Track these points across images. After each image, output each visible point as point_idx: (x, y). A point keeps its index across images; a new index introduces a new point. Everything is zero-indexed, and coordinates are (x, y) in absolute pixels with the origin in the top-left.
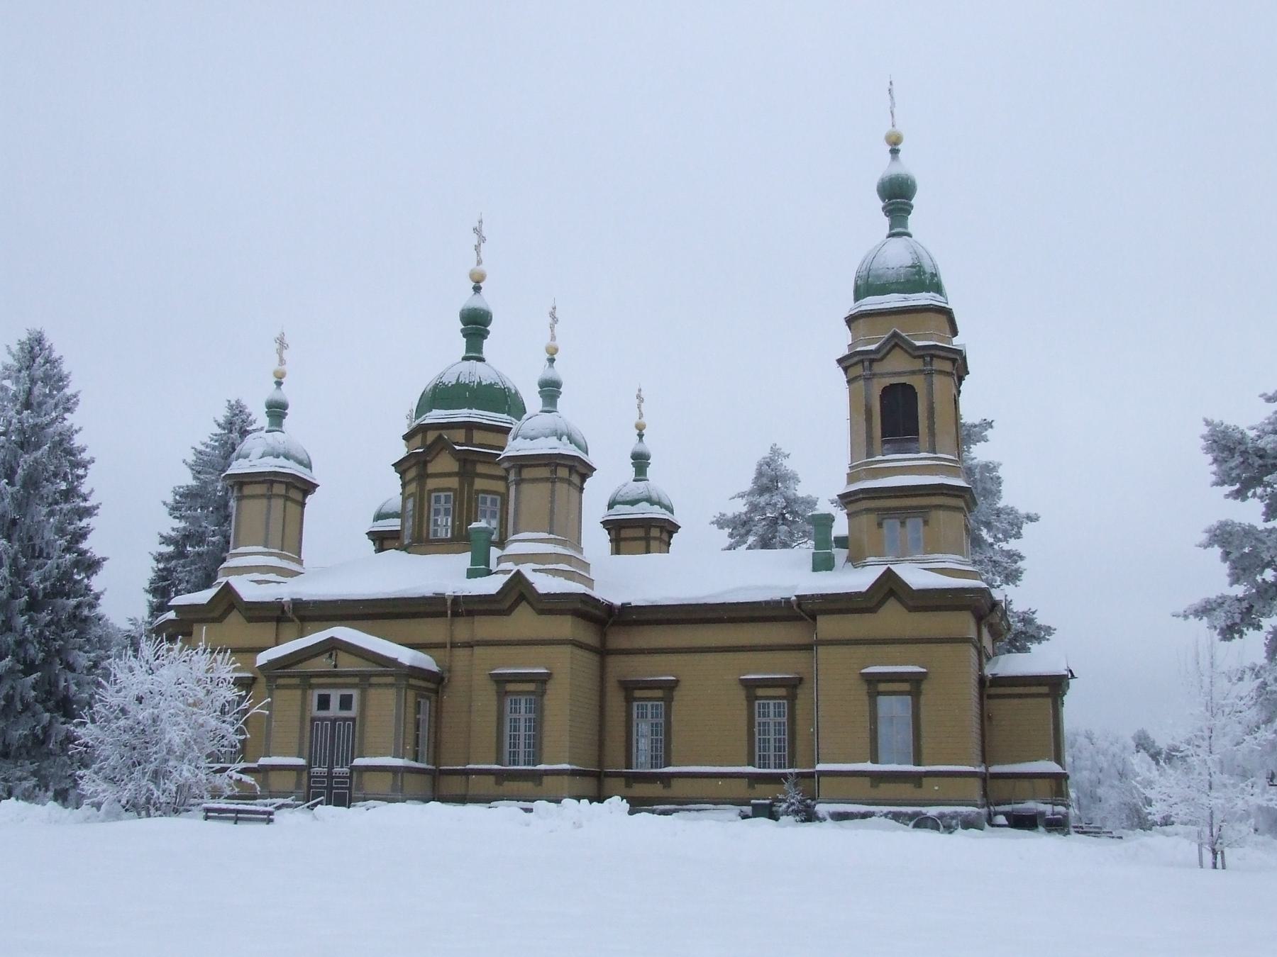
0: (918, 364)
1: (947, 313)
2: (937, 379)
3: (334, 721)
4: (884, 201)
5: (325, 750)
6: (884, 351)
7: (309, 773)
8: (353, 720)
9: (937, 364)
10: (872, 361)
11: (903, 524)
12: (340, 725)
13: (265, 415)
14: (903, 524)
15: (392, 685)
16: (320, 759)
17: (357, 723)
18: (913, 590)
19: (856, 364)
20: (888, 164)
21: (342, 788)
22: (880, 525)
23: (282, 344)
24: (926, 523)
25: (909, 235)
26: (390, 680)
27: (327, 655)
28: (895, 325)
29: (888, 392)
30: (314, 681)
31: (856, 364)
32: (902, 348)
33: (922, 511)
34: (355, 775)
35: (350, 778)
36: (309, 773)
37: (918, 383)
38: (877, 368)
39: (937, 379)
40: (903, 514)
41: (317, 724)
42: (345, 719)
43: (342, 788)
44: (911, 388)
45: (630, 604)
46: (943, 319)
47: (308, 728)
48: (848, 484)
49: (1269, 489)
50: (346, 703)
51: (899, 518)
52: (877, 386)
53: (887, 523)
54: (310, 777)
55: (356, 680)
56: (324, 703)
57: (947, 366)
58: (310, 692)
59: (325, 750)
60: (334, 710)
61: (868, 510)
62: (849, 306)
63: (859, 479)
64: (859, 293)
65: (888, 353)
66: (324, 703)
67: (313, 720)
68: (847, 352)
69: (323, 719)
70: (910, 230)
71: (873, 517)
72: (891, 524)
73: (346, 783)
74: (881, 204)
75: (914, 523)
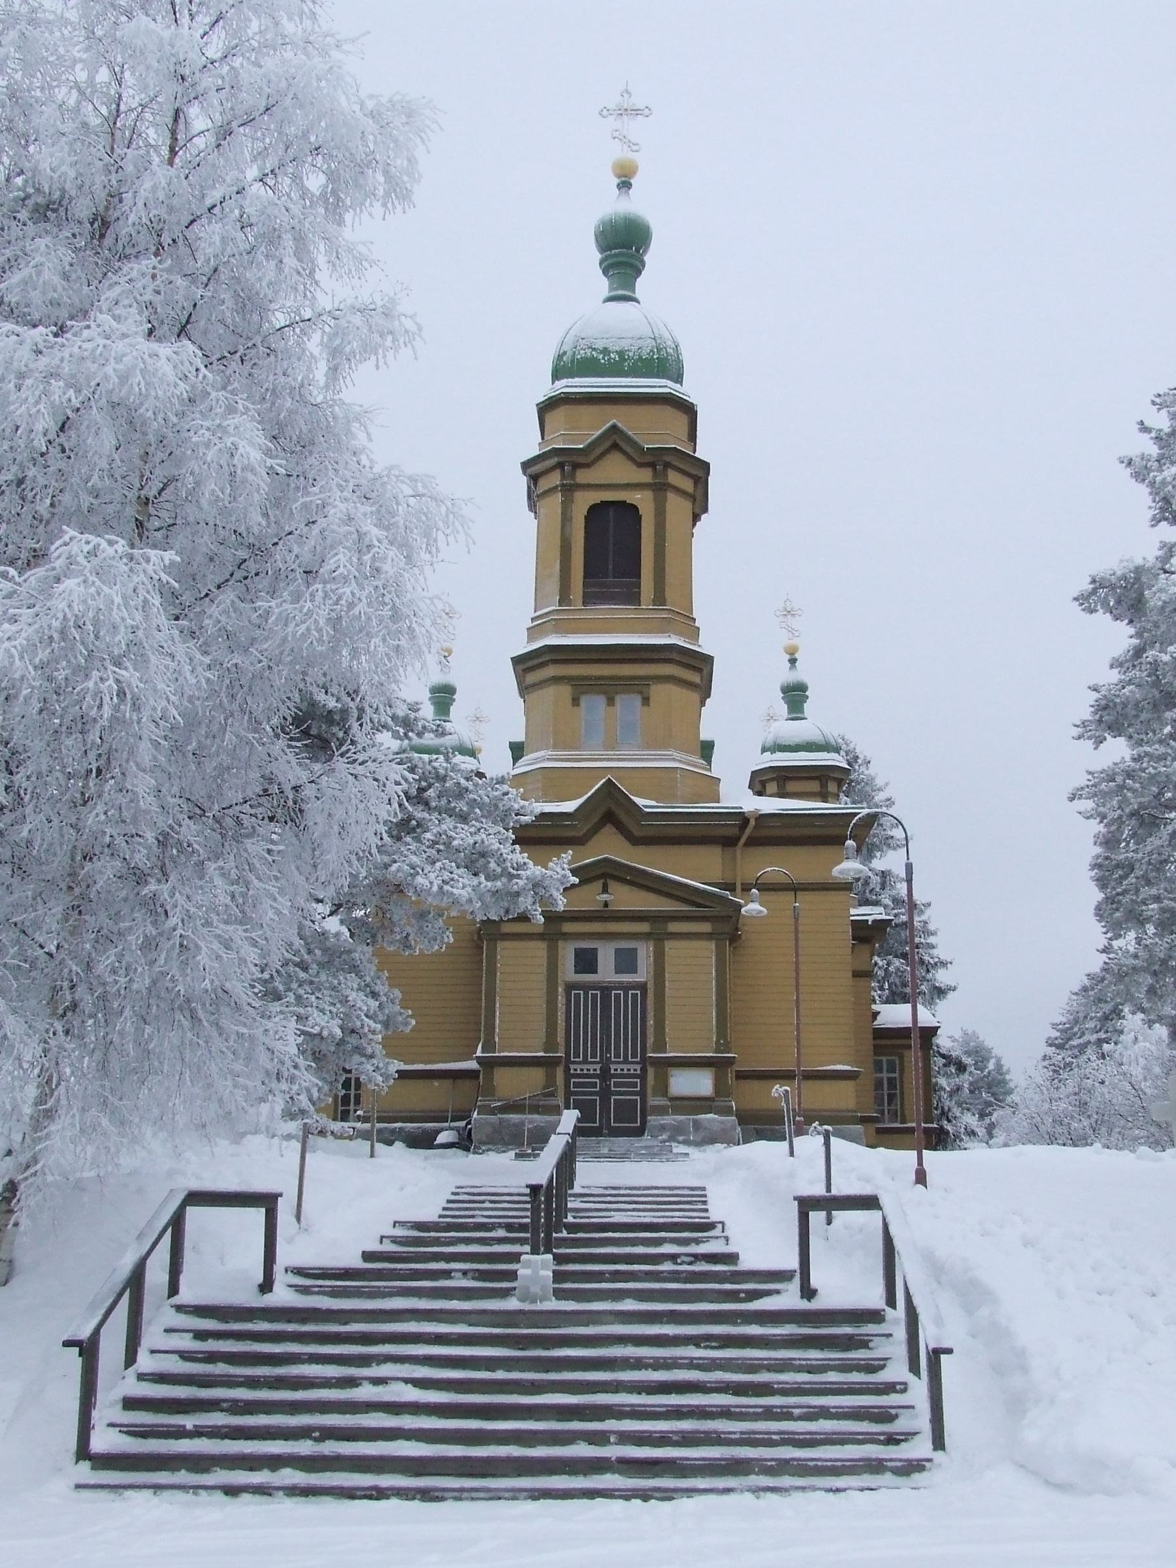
0: (646, 475)
1: (688, 410)
2: (672, 499)
3: (606, 989)
4: (601, 253)
6: (598, 451)
7: (567, 1069)
8: (643, 987)
9: (674, 478)
10: (576, 466)
11: (611, 702)
12: (617, 996)
13: (782, 701)
14: (611, 702)
15: (708, 936)
19: (552, 469)
22: (576, 702)
24: (646, 701)
25: (636, 300)
26: (706, 927)
27: (600, 883)
28: (615, 417)
29: (596, 512)
31: (552, 469)
32: (625, 453)
33: (640, 687)
34: (651, 1072)
35: (643, 1076)
36: (567, 1069)
37: (642, 500)
38: (582, 476)
39: (672, 499)
40: (610, 689)
41: (577, 996)
42: (626, 987)
44: (634, 509)
46: (683, 420)
47: (561, 999)
48: (528, 642)
50: (626, 962)
51: (605, 693)
52: (584, 501)
53: (584, 700)
54: (568, 1075)
55: (644, 927)
56: (587, 961)
57: (687, 485)
58: (561, 944)
60: (606, 971)
61: (557, 680)
62: (545, 388)
63: (545, 634)
64: (557, 375)
65: (603, 455)
66: (626, 962)
67: (569, 987)
68: (537, 452)
69: (586, 987)
70: (638, 295)
71: (566, 691)
72: (595, 704)
73: (576, 1085)
74: (599, 256)
75: (628, 705)
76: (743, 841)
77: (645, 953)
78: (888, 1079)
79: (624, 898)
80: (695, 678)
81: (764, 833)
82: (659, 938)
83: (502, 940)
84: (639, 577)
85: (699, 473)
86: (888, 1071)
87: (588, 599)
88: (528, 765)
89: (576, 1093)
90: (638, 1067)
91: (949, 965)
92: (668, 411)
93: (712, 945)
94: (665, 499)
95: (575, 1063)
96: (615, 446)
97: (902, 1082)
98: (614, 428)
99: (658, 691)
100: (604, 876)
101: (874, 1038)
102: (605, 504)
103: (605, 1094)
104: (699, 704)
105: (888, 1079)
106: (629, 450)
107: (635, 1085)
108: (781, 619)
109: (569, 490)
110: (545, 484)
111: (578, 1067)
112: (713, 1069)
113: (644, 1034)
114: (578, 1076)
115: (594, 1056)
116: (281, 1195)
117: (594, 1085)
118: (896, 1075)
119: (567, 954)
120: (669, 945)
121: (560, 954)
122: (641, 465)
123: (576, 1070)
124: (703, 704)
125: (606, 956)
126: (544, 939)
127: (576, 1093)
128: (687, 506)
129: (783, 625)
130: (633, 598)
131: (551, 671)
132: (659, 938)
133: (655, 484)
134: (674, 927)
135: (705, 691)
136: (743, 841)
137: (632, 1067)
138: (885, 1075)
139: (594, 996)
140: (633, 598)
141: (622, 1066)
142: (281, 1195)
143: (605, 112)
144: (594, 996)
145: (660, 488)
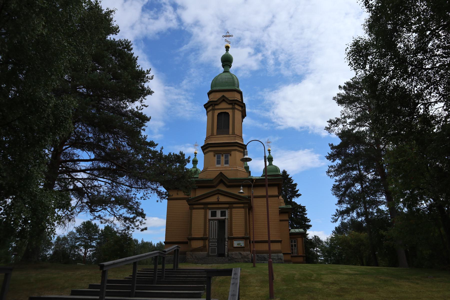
0: (230, 106)
1: (241, 93)
9: (237, 107)
15: (243, 208)
26: (242, 205)
29: (219, 114)
30: (209, 206)
37: (230, 112)
38: (217, 107)
39: (236, 111)
44: (228, 113)
50: (223, 214)
52: (217, 112)
54: (209, 242)
55: (227, 206)
56: (214, 214)
57: (240, 108)
58: (208, 210)
67: (210, 220)
77: (227, 212)
78: (294, 244)
79: (223, 199)
80: (242, 150)
81: (257, 183)
82: (230, 208)
83: (193, 209)
86: (294, 243)
88: (355, 271)
89: (211, 246)
92: (236, 93)
93: (243, 209)
94: (235, 111)
96: (224, 100)
97: (297, 245)
98: (223, 96)
99: (233, 153)
102: (221, 113)
105: (294, 244)
106: (227, 101)
109: (214, 110)
110: (209, 109)
114: (212, 242)
115: (216, 237)
119: (209, 213)
122: (229, 104)
125: (219, 213)
127: (211, 246)
130: (228, 133)
131: (210, 149)
134: (235, 205)
138: (293, 244)
140: (228, 133)
143: (223, 36)
145: (233, 109)
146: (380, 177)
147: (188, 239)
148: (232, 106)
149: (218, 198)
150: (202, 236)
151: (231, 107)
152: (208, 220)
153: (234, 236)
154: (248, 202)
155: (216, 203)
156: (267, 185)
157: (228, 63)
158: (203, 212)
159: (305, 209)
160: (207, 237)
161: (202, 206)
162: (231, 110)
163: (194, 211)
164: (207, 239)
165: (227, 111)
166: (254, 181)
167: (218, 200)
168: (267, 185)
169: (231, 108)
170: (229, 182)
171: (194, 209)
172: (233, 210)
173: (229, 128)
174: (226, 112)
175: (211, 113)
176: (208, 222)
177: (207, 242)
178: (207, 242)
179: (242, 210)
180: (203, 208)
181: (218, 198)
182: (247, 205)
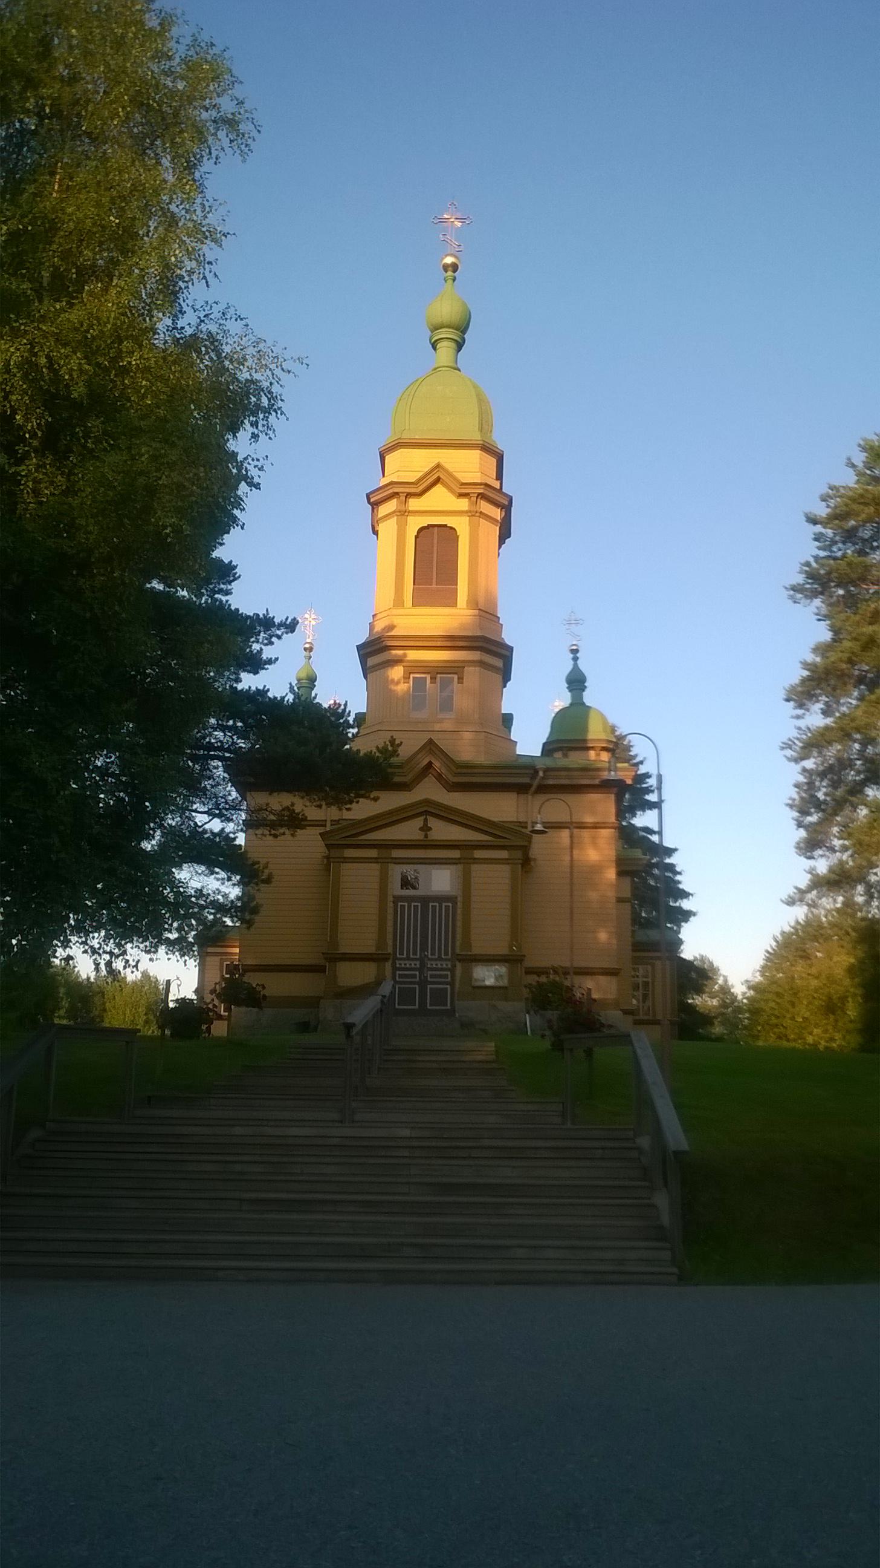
0: (464, 504)
5: (415, 935)
13: (567, 690)
16: (440, 948)
17: (459, 905)
18: (571, 704)
20: (469, 306)
21: (411, 983)
23: (575, 652)
26: (504, 854)
30: (396, 853)
34: (459, 965)
35: (452, 970)
36: (394, 964)
37: (462, 526)
38: (414, 504)
41: (403, 907)
43: (411, 983)
45: (796, 852)
47: (390, 911)
49: (837, 714)
52: (415, 524)
54: (395, 969)
55: (456, 854)
58: (391, 866)
59: (415, 935)
67: (397, 899)
69: (410, 899)
76: (533, 789)
79: (442, 831)
80: (499, 663)
84: (457, 584)
85: (508, 654)
87: (415, 604)
90: (418, 963)
91: (691, 897)
95: (432, 960)
97: (653, 984)
100: (427, 813)
101: (633, 951)
102: (430, 526)
103: (423, 983)
104: (501, 684)
105: (643, 982)
107: (446, 976)
108: (567, 626)
111: (434, 963)
112: (507, 964)
113: (454, 937)
115: (415, 953)
116: (694, 914)
117: (414, 976)
118: (650, 980)
120: (474, 867)
121: (390, 873)
123: (400, 964)
124: (505, 686)
126: (377, 862)
128: (499, 678)
129: (568, 631)
132: (466, 862)
133: (470, 512)
134: (478, 854)
135: (506, 677)
136: (533, 789)
137: (413, 963)
139: (416, 907)
141: (406, 962)
142: (694, 914)
144: (416, 907)
145: (472, 514)
146: (147, 846)
147: (326, 959)
148: (471, 504)
149: (426, 828)
150: (372, 950)
151: (466, 508)
152: (390, 898)
153: (477, 950)
154: (523, 846)
155: (417, 843)
156: (328, 824)
157: (439, 334)
158: (377, 873)
159: (671, 868)
160: (389, 954)
161: (373, 853)
162: (465, 520)
163: (347, 869)
164: (386, 960)
165: (449, 521)
166: (541, 774)
167: (426, 836)
168: (328, 824)
169: (466, 512)
170: (456, 774)
171: (347, 860)
172: (474, 867)
173: (455, 582)
174: (445, 526)
175: (396, 527)
176: (650, 975)
177: (388, 966)
178: (388, 966)
179: (505, 870)
180: (375, 860)
181: (426, 828)
182: (519, 854)
